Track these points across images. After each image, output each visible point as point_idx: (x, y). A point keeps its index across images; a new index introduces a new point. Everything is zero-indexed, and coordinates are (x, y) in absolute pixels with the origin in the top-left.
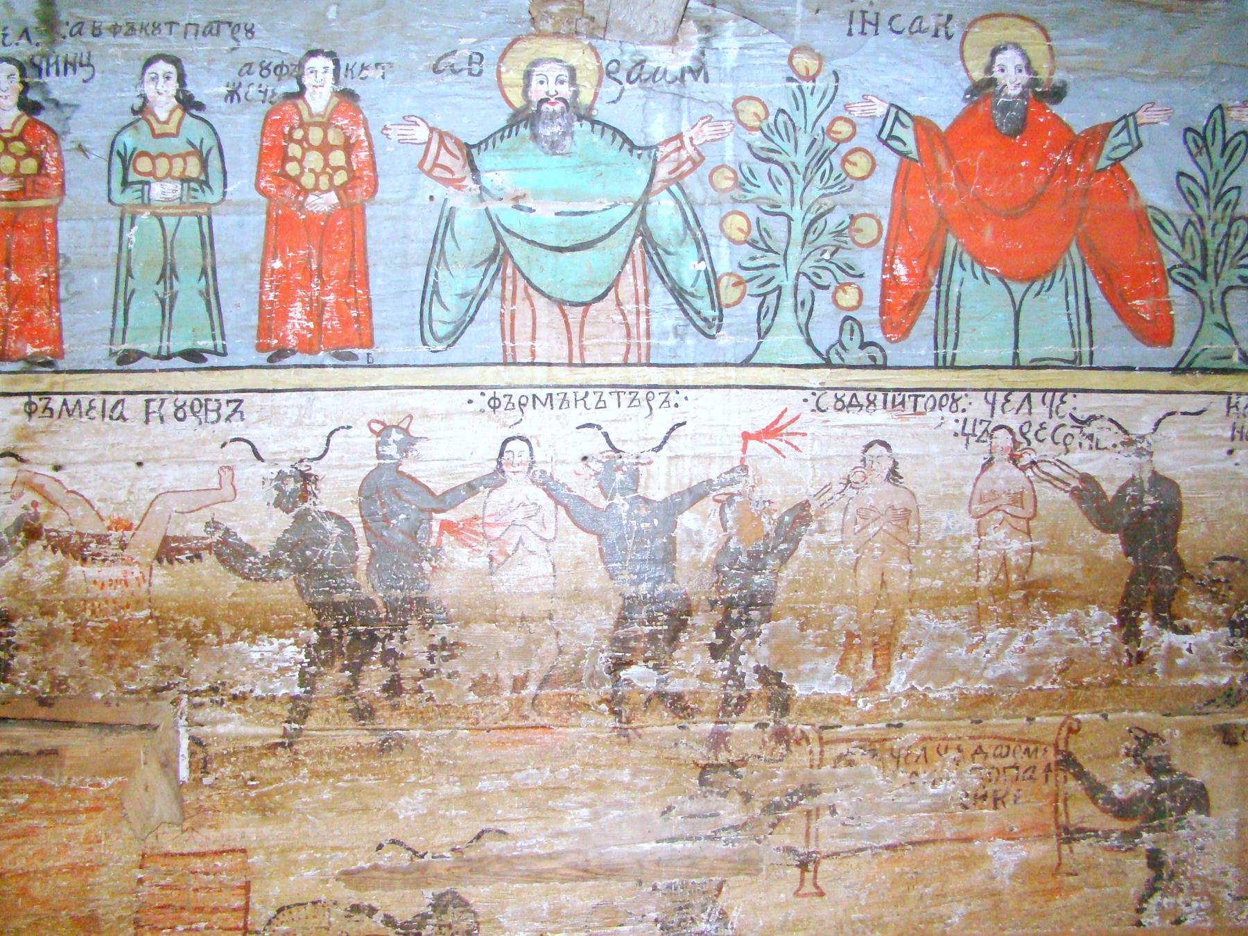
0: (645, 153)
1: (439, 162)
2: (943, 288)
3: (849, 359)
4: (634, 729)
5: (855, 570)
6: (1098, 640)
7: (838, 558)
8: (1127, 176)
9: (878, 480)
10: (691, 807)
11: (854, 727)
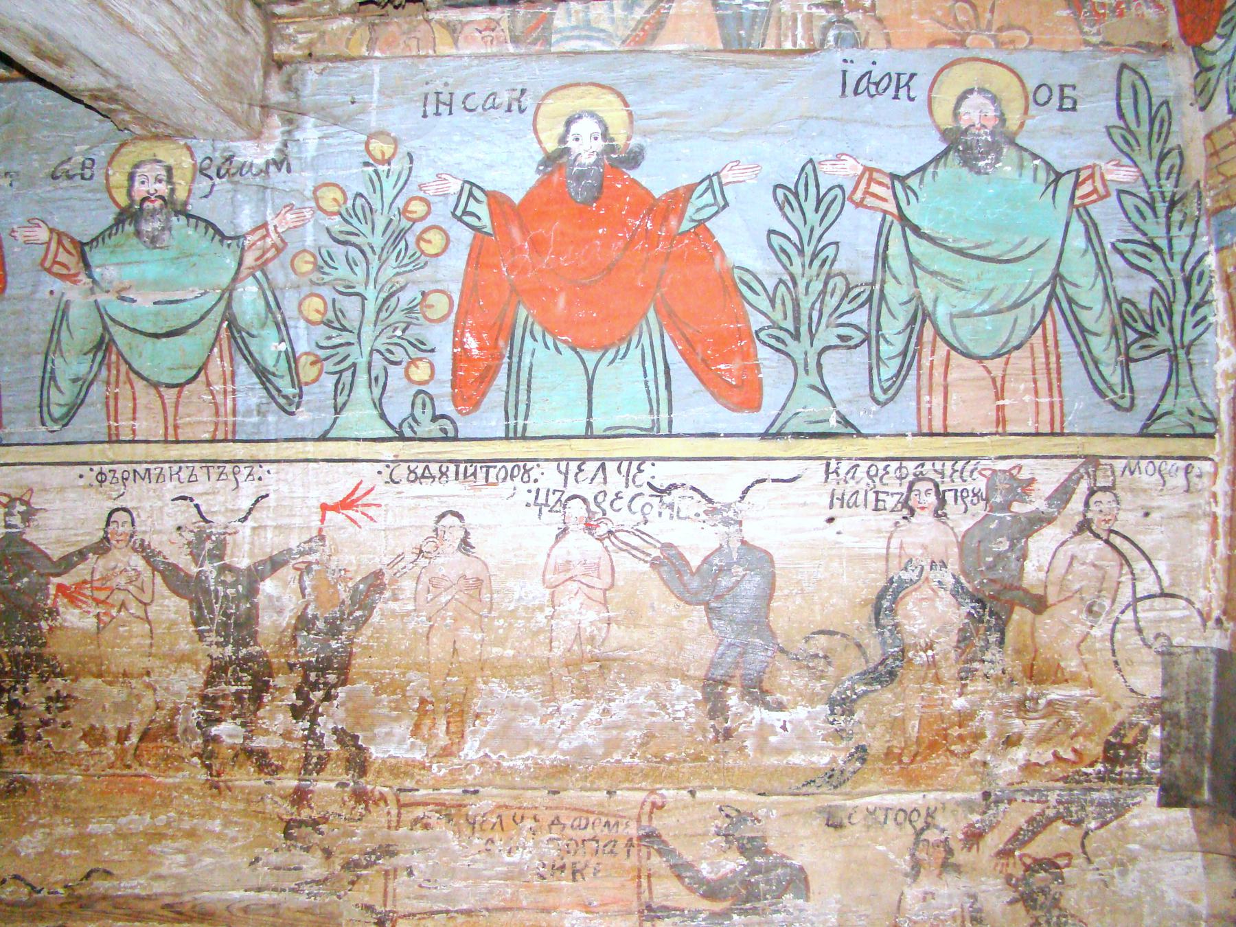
0: (234, 243)
1: (58, 259)
2: (515, 359)
3: (421, 431)
4: (225, 781)
5: (428, 638)
6: (682, 714)
7: (411, 626)
8: (713, 237)
9: (450, 550)
10: (275, 858)
11: (431, 791)
